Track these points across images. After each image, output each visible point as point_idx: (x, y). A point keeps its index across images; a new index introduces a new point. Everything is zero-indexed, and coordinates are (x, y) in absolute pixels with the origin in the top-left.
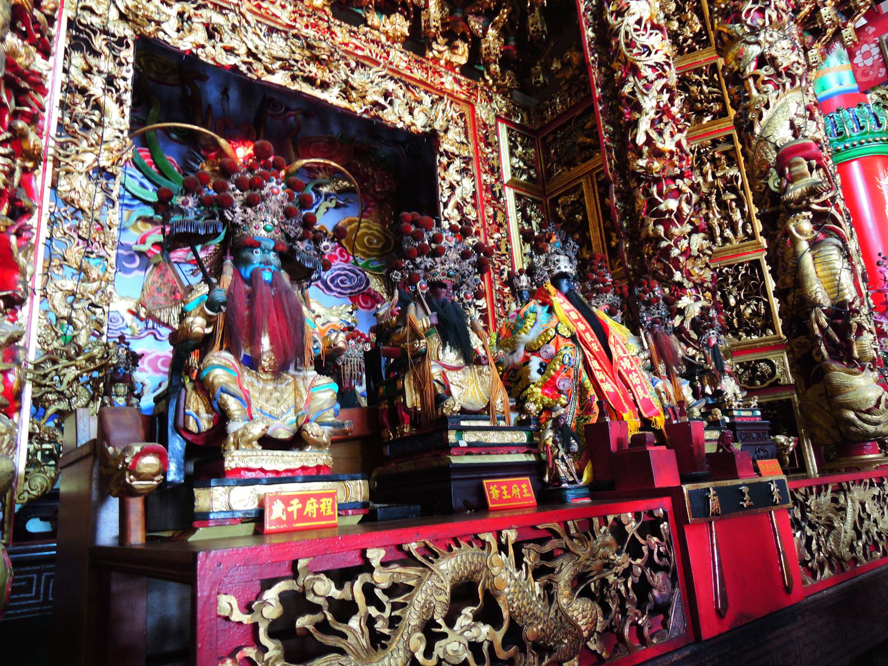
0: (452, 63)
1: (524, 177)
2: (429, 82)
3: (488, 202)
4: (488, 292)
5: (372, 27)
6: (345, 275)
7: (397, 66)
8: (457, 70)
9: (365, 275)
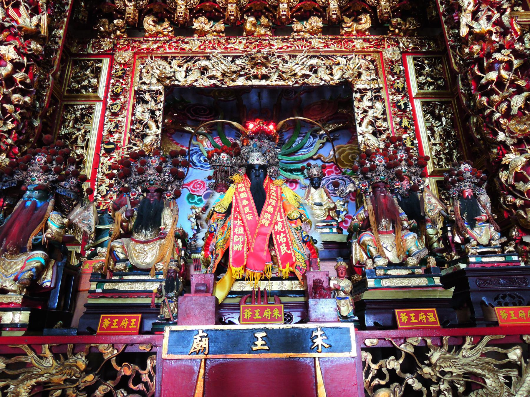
0: (360, 30)
1: (432, 87)
2: (343, 49)
3: (395, 114)
5: (298, 31)
7: (318, 48)
8: (367, 33)
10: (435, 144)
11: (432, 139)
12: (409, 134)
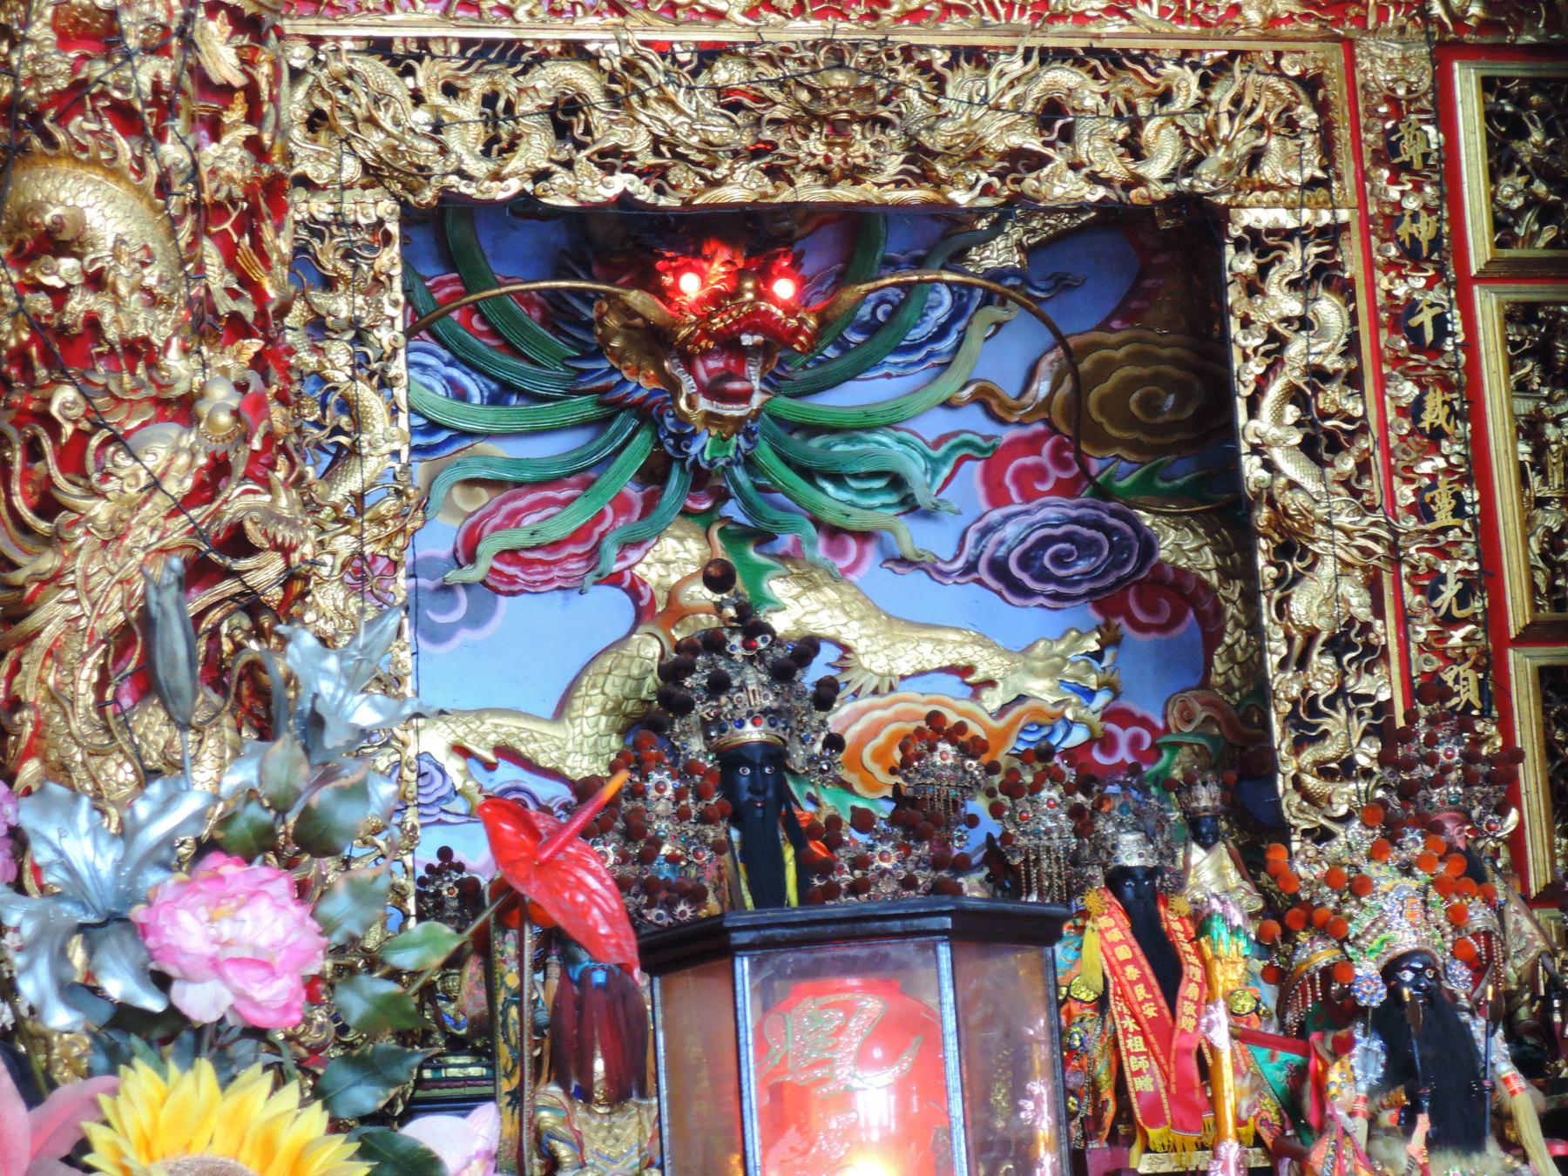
3: (1398, 361)
4: (1394, 650)
6: (1066, 538)
9: (1135, 524)
10: (1541, 502)
11: (1535, 480)
12: (1446, 457)
